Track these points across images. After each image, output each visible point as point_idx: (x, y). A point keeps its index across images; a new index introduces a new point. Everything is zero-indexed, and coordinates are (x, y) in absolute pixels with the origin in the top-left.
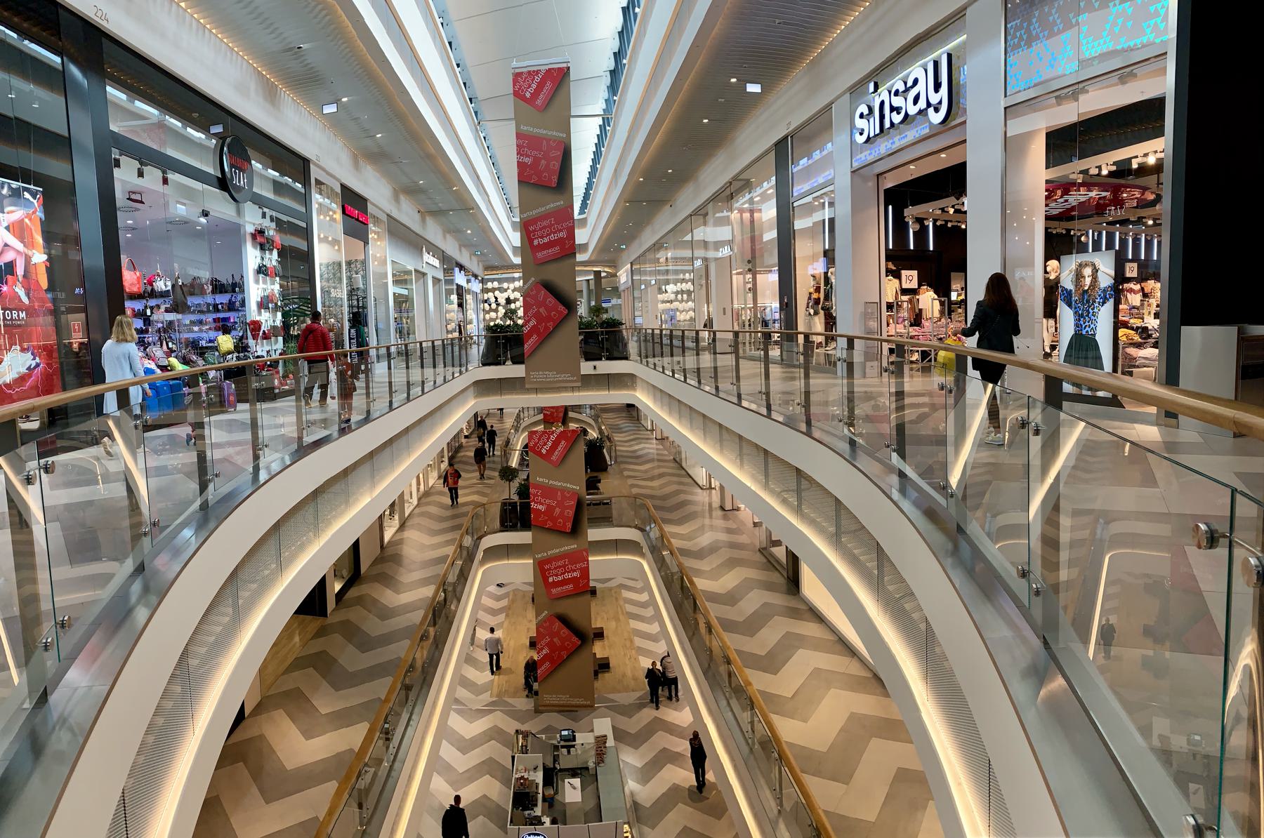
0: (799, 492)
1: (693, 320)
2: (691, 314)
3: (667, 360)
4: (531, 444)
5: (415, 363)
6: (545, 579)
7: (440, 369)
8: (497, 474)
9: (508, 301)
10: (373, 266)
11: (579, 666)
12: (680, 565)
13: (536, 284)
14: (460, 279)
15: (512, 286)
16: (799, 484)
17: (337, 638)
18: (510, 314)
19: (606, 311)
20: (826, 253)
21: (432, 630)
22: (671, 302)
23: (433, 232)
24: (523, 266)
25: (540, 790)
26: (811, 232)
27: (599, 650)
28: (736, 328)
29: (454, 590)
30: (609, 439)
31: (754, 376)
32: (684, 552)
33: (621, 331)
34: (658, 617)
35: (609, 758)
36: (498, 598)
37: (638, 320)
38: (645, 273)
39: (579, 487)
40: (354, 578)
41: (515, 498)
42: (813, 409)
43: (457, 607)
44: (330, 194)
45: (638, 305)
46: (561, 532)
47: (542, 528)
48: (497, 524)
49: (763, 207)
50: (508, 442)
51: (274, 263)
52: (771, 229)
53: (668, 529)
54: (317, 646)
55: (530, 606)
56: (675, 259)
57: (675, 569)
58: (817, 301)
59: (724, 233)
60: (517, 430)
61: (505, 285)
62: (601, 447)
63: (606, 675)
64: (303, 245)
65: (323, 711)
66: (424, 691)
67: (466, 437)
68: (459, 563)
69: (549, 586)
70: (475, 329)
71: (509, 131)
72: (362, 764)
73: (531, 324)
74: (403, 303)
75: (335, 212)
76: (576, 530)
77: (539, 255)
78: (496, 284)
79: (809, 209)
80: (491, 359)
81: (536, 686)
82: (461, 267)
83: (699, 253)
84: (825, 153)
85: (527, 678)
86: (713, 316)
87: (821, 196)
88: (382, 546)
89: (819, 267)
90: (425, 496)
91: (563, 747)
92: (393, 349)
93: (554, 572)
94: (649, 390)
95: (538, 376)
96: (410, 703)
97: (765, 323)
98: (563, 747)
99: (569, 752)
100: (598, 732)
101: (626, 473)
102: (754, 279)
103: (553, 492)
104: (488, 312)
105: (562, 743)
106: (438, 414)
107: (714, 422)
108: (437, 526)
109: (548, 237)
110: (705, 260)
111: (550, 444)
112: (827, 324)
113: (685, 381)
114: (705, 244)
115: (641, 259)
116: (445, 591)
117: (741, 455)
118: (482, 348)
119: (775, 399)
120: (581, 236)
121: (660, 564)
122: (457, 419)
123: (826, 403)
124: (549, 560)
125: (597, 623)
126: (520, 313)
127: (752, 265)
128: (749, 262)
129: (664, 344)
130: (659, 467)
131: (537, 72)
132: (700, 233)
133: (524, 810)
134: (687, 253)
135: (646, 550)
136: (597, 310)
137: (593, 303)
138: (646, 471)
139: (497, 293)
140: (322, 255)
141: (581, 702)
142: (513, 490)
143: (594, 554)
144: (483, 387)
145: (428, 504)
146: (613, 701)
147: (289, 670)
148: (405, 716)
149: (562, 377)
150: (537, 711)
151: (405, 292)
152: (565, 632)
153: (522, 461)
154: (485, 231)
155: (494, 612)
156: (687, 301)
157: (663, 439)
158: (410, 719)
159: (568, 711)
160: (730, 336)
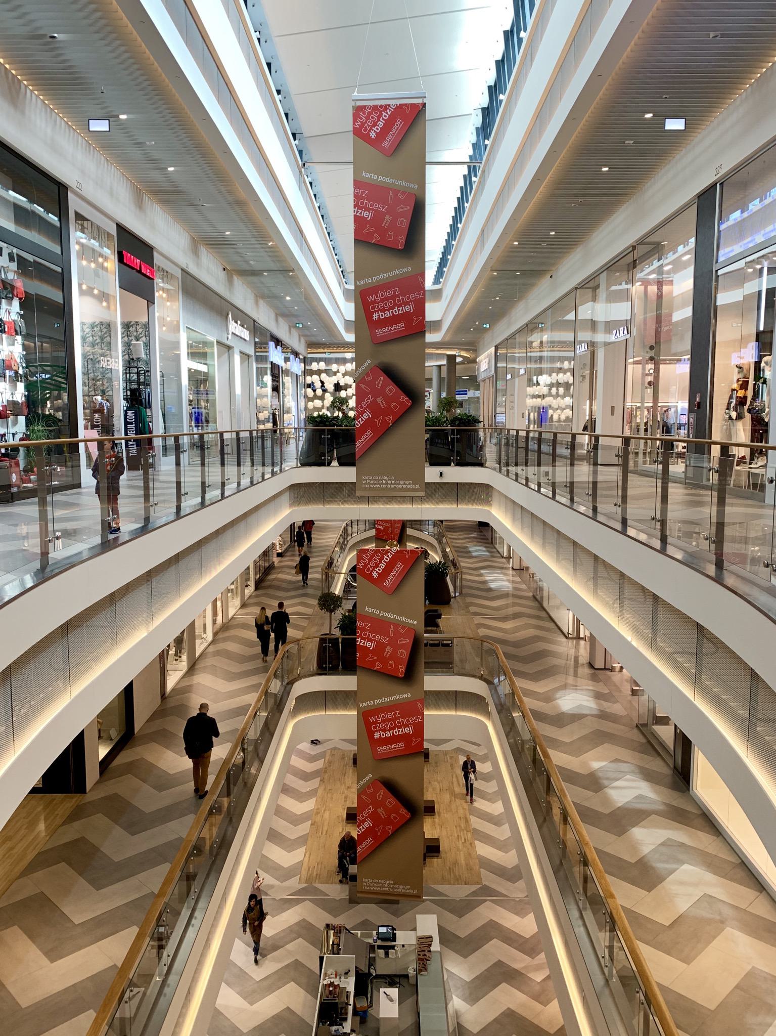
0: (698, 656)
1: (569, 420)
2: (568, 412)
3: (532, 470)
4: (361, 566)
5: (213, 459)
6: (370, 734)
7: (246, 468)
8: (315, 602)
9: (338, 387)
10: (158, 332)
11: (405, 847)
12: (532, 732)
13: (372, 370)
14: (276, 356)
15: (342, 369)
16: (699, 644)
17: (100, 820)
18: (339, 403)
19: (461, 404)
20: (759, 336)
21: (225, 801)
22: (543, 397)
23: (241, 295)
24: (356, 346)
25: (351, 1002)
26: (740, 309)
27: (430, 829)
28: (627, 433)
29: (256, 749)
30: (455, 565)
31: (647, 496)
32: (540, 716)
33: (476, 431)
34: (502, 793)
35: (433, 966)
36: (312, 759)
37: (500, 418)
38: (513, 359)
39: (416, 622)
40: (126, 739)
41: (337, 633)
42: (728, 548)
43: (259, 770)
44: (98, 232)
45: (501, 399)
46: (391, 677)
47: (369, 670)
48: (314, 666)
49: (676, 278)
50: (330, 564)
51: (14, 317)
52: (684, 306)
53: (521, 684)
54: (71, 833)
55: (350, 770)
56: (552, 343)
57: (527, 736)
58: (742, 401)
59: (620, 311)
60: (342, 548)
61: (334, 367)
62: (444, 575)
63: (435, 860)
64: (56, 295)
65: (78, 919)
66: (207, 888)
67: (279, 555)
68: (264, 714)
69: (374, 325)
70: (293, 420)
71: (347, 175)
72: (125, 983)
73: (365, 416)
74: (200, 382)
75: (106, 259)
76: (410, 676)
77: (379, 332)
78: (322, 365)
79: (740, 278)
80: (314, 456)
81: (353, 869)
82: (278, 342)
83: (585, 335)
84: (745, 215)
85: (341, 858)
86: (598, 417)
87: (758, 261)
88: (163, 696)
89: (748, 355)
90: (224, 630)
91: (380, 947)
92: (185, 440)
93: (382, 726)
94: (517, 518)
95: (372, 482)
96: (193, 896)
97: (667, 429)
98: (380, 947)
99: (387, 954)
100: (421, 932)
101: (473, 609)
102: (657, 370)
103: (381, 630)
104: (312, 399)
105: (379, 943)
106: (242, 525)
107: (589, 552)
108: (235, 668)
109: (391, 313)
110: (592, 345)
111: (383, 565)
112: (754, 431)
113: (554, 498)
114: (593, 325)
115: (509, 342)
116: (243, 750)
117: (621, 600)
118: (301, 444)
119: (673, 529)
120: (432, 311)
121: (509, 728)
122: (269, 530)
123: (746, 540)
124: (375, 711)
125: (429, 796)
126: (352, 403)
127: (655, 352)
128: (652, 348)
129: (533, 449)
130: (514, 604)
131: (386, 107)
132: (586, 311)
133: (331, 1025)
134: (568, 336)
135: (492, 708)
136: (447, 404)
137: (444, 395)
138: (496, 609)
139: (323, 376)
140: (84, 312)
141: (407, 890)
142: (335, 623)
143: (429, 709)
144: (302, 492)
145: (225, 640)
146: (441, 894)
147: (31, 868)
148: (185, 913)
149: (402, 484)
150: (353, 900)
151: (203, 368)
152: (391, 801)
153: (348, 588)
154: (309, 297)
155: (306, 777)
156: (564, 396)
157: (521, 570)
158: (191, 917)
159: (389, 901)
160: (619, 443)
